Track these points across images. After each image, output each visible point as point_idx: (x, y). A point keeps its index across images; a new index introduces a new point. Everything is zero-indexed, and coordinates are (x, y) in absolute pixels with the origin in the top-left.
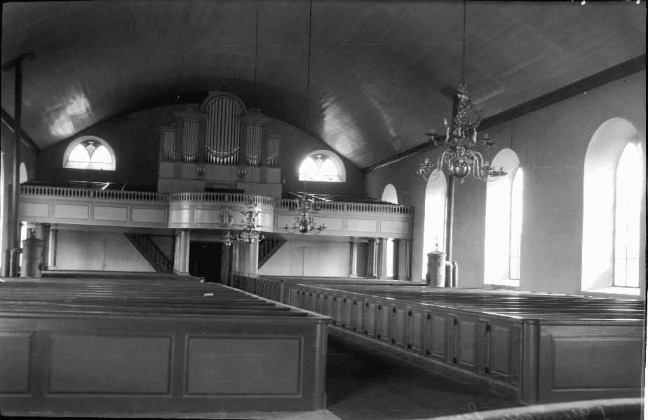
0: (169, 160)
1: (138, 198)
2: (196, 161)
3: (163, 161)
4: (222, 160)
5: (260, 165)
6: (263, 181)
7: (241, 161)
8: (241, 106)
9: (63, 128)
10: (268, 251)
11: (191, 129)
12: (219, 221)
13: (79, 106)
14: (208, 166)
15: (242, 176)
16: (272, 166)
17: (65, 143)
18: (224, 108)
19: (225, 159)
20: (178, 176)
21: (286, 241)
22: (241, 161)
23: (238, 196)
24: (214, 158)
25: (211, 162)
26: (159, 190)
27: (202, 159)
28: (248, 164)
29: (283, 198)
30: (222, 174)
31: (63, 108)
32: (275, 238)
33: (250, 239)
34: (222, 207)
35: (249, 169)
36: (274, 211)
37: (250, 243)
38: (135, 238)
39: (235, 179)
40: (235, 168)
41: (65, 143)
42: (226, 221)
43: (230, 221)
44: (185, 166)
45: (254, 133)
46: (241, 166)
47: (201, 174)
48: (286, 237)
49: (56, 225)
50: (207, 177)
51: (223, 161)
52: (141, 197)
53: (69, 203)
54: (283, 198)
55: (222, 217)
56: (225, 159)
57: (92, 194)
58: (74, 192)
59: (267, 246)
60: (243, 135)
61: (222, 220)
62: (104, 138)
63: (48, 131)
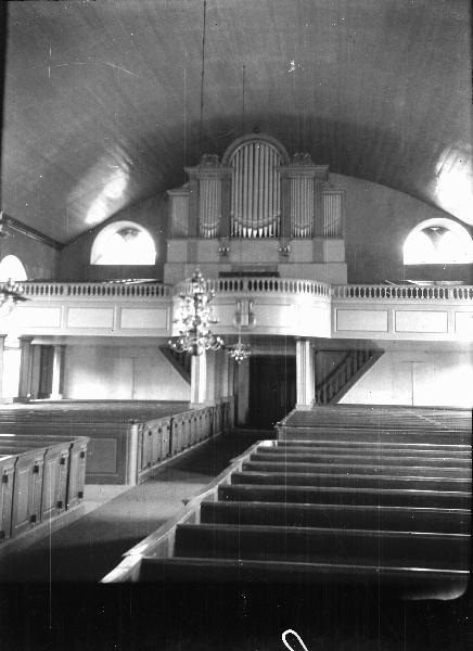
0: (180, 236)
1: (84, 292)
2: (218, 236)
3: (189, 244)
4: (255, 233)
5: (312, 236)
6: (318, 259)
7: (283, 232)
8: (281, 152)
9: (95, 213)
10: (352, 374)
11: (210, 189)
12: (235, 322)
13: (114, 187)
14: (235, 244)
15: (284, 254)
16: (331, 236)
17: (95, 230)
18: (257, 162)
19: (261, 231)
20: (192, 260)
21: (383, 352)
22: (283, 232)
23: (258, 281)
24: (250, 231)
25: (238, 236)
26: (165, 282)
27: (227, 232)
28: (296, 236)
29: (350, 282)
30: (254, 253)
31: (99, 189)
32: (367, 348)
33: (195, 347)
34: (239, 300)
35: (295, 242)
36: (332, 304)
37: (195, 353)
38: (177, 359)
39: (275, 258)
40: (276, 244)
41: (95, 230)
42: (245, 321)
43: (251, 320)
44: (201, 243)
45: (303, 191)
46: (284, 240)
47: (225, 254)
48: (380, 346)
49: (64, 337)
50: (234, 258)
51: (258, 235)
52: (150, 291)
53: (86, 306)
54: (350, 282)
55: (238, 316)
56: (261, 231)
57: (66, 290)
58: (47, 288)
59: (355, 361)
60: (285, 191)
61: (239, 320)
62: (144, 226)
63: (81, 222)
